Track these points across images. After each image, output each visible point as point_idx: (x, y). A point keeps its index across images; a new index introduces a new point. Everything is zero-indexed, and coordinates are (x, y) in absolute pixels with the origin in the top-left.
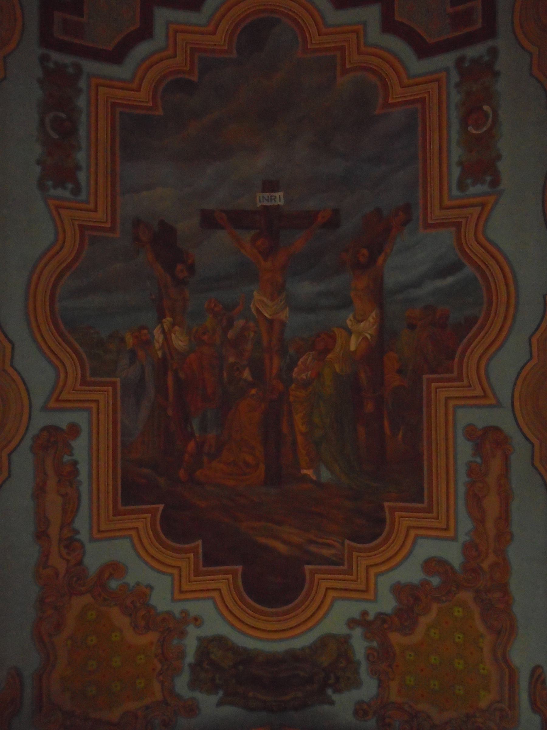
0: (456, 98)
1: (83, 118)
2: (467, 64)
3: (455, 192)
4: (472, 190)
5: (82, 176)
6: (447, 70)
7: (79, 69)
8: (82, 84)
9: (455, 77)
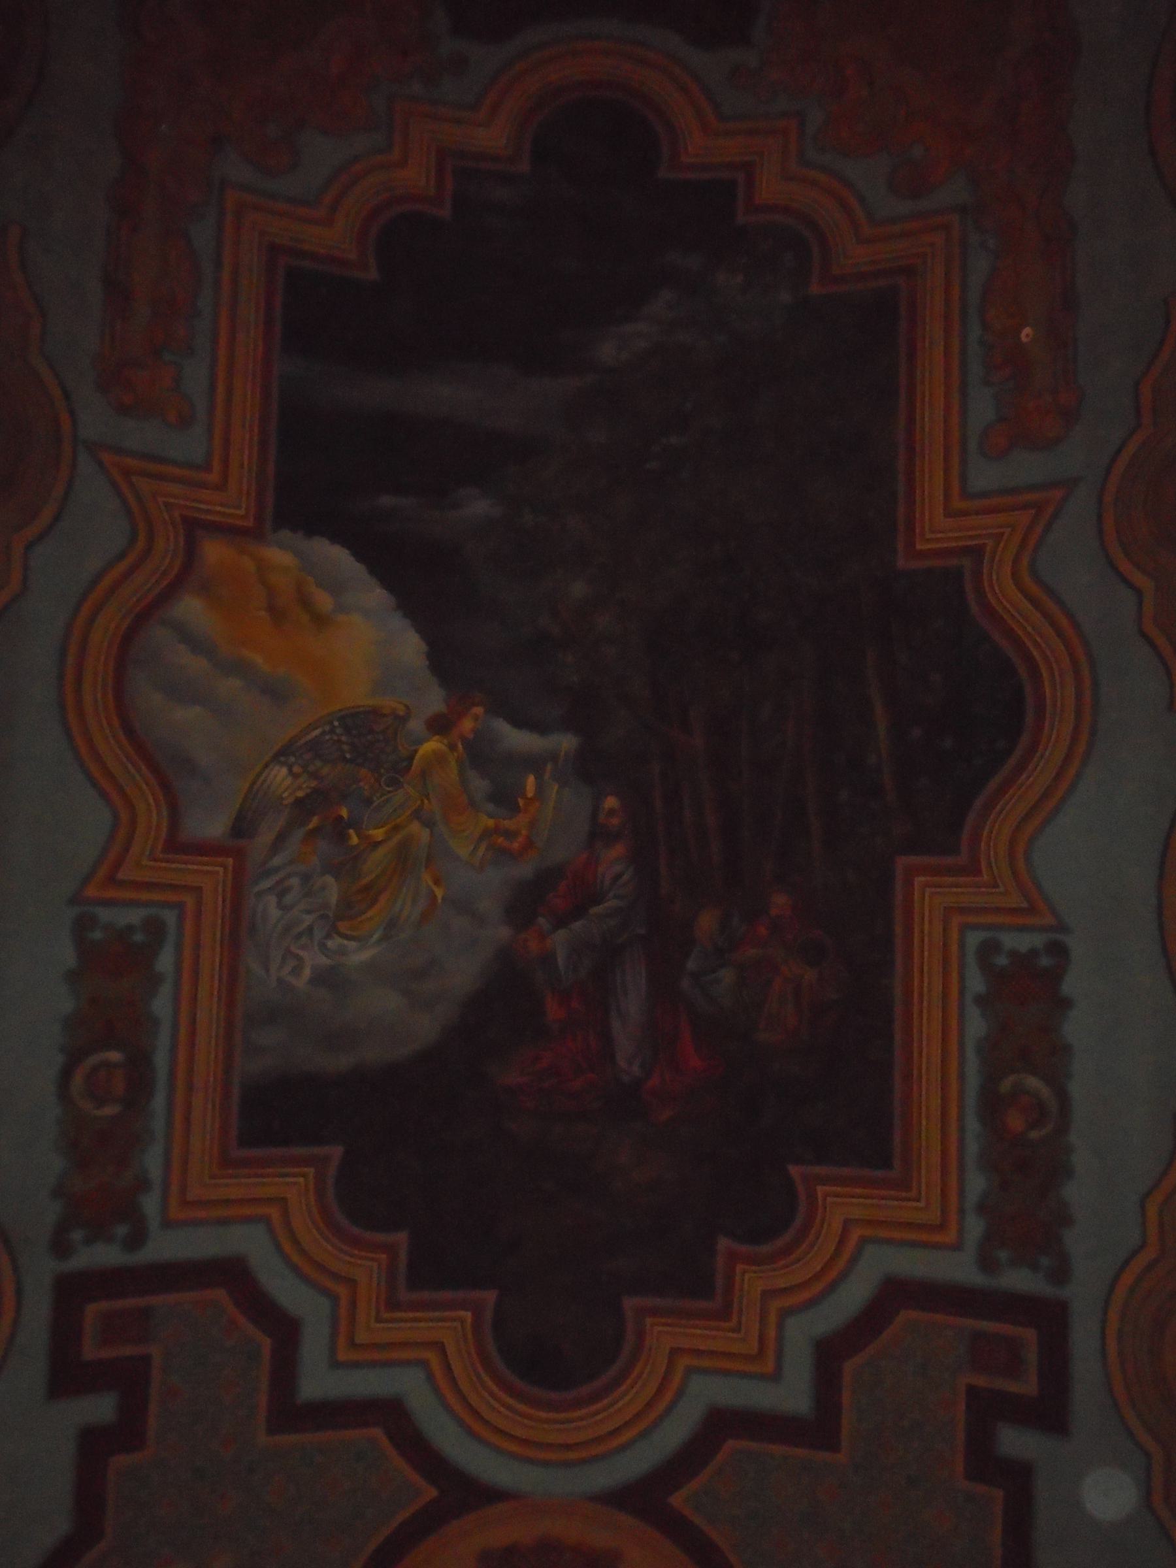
0: (152, 1161)
1: (973, 1148)
2: (122, 1230)
3: (170, 917)
4: (134, 917)
5: (976, 984)
6: (168, 1224)
7: (987, 1263)
8: (975, 1227)
9: (150, 1204)
